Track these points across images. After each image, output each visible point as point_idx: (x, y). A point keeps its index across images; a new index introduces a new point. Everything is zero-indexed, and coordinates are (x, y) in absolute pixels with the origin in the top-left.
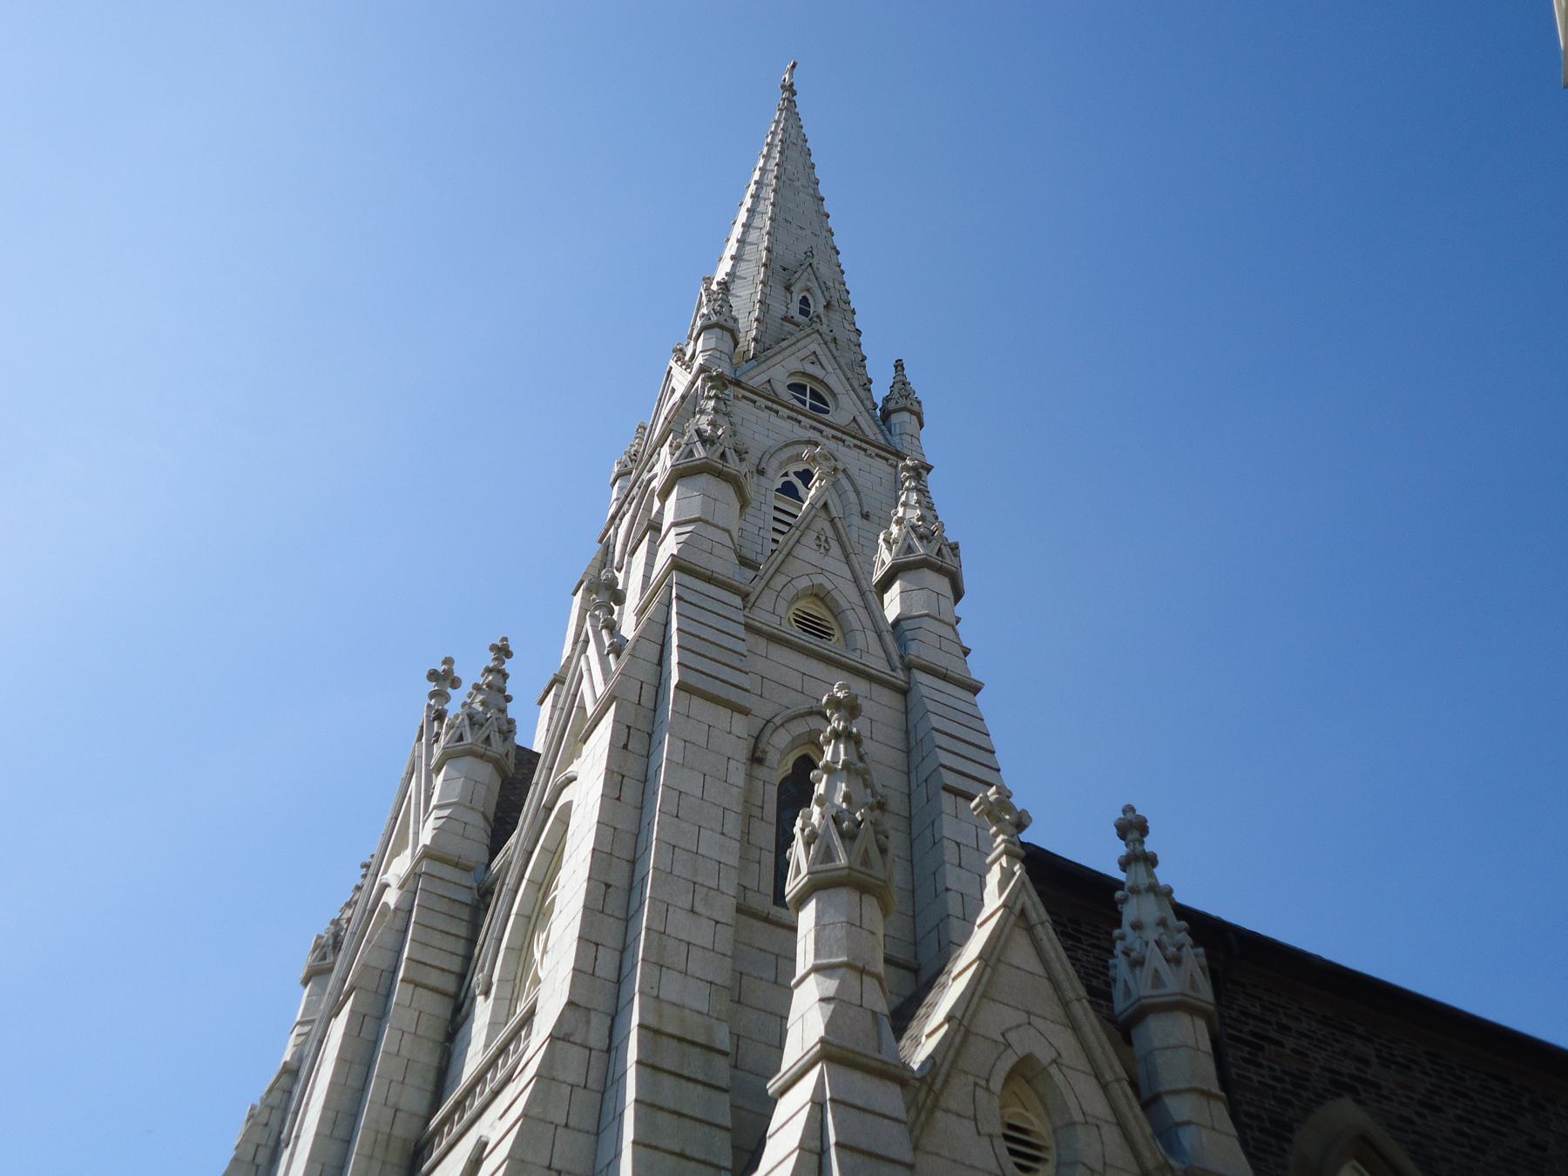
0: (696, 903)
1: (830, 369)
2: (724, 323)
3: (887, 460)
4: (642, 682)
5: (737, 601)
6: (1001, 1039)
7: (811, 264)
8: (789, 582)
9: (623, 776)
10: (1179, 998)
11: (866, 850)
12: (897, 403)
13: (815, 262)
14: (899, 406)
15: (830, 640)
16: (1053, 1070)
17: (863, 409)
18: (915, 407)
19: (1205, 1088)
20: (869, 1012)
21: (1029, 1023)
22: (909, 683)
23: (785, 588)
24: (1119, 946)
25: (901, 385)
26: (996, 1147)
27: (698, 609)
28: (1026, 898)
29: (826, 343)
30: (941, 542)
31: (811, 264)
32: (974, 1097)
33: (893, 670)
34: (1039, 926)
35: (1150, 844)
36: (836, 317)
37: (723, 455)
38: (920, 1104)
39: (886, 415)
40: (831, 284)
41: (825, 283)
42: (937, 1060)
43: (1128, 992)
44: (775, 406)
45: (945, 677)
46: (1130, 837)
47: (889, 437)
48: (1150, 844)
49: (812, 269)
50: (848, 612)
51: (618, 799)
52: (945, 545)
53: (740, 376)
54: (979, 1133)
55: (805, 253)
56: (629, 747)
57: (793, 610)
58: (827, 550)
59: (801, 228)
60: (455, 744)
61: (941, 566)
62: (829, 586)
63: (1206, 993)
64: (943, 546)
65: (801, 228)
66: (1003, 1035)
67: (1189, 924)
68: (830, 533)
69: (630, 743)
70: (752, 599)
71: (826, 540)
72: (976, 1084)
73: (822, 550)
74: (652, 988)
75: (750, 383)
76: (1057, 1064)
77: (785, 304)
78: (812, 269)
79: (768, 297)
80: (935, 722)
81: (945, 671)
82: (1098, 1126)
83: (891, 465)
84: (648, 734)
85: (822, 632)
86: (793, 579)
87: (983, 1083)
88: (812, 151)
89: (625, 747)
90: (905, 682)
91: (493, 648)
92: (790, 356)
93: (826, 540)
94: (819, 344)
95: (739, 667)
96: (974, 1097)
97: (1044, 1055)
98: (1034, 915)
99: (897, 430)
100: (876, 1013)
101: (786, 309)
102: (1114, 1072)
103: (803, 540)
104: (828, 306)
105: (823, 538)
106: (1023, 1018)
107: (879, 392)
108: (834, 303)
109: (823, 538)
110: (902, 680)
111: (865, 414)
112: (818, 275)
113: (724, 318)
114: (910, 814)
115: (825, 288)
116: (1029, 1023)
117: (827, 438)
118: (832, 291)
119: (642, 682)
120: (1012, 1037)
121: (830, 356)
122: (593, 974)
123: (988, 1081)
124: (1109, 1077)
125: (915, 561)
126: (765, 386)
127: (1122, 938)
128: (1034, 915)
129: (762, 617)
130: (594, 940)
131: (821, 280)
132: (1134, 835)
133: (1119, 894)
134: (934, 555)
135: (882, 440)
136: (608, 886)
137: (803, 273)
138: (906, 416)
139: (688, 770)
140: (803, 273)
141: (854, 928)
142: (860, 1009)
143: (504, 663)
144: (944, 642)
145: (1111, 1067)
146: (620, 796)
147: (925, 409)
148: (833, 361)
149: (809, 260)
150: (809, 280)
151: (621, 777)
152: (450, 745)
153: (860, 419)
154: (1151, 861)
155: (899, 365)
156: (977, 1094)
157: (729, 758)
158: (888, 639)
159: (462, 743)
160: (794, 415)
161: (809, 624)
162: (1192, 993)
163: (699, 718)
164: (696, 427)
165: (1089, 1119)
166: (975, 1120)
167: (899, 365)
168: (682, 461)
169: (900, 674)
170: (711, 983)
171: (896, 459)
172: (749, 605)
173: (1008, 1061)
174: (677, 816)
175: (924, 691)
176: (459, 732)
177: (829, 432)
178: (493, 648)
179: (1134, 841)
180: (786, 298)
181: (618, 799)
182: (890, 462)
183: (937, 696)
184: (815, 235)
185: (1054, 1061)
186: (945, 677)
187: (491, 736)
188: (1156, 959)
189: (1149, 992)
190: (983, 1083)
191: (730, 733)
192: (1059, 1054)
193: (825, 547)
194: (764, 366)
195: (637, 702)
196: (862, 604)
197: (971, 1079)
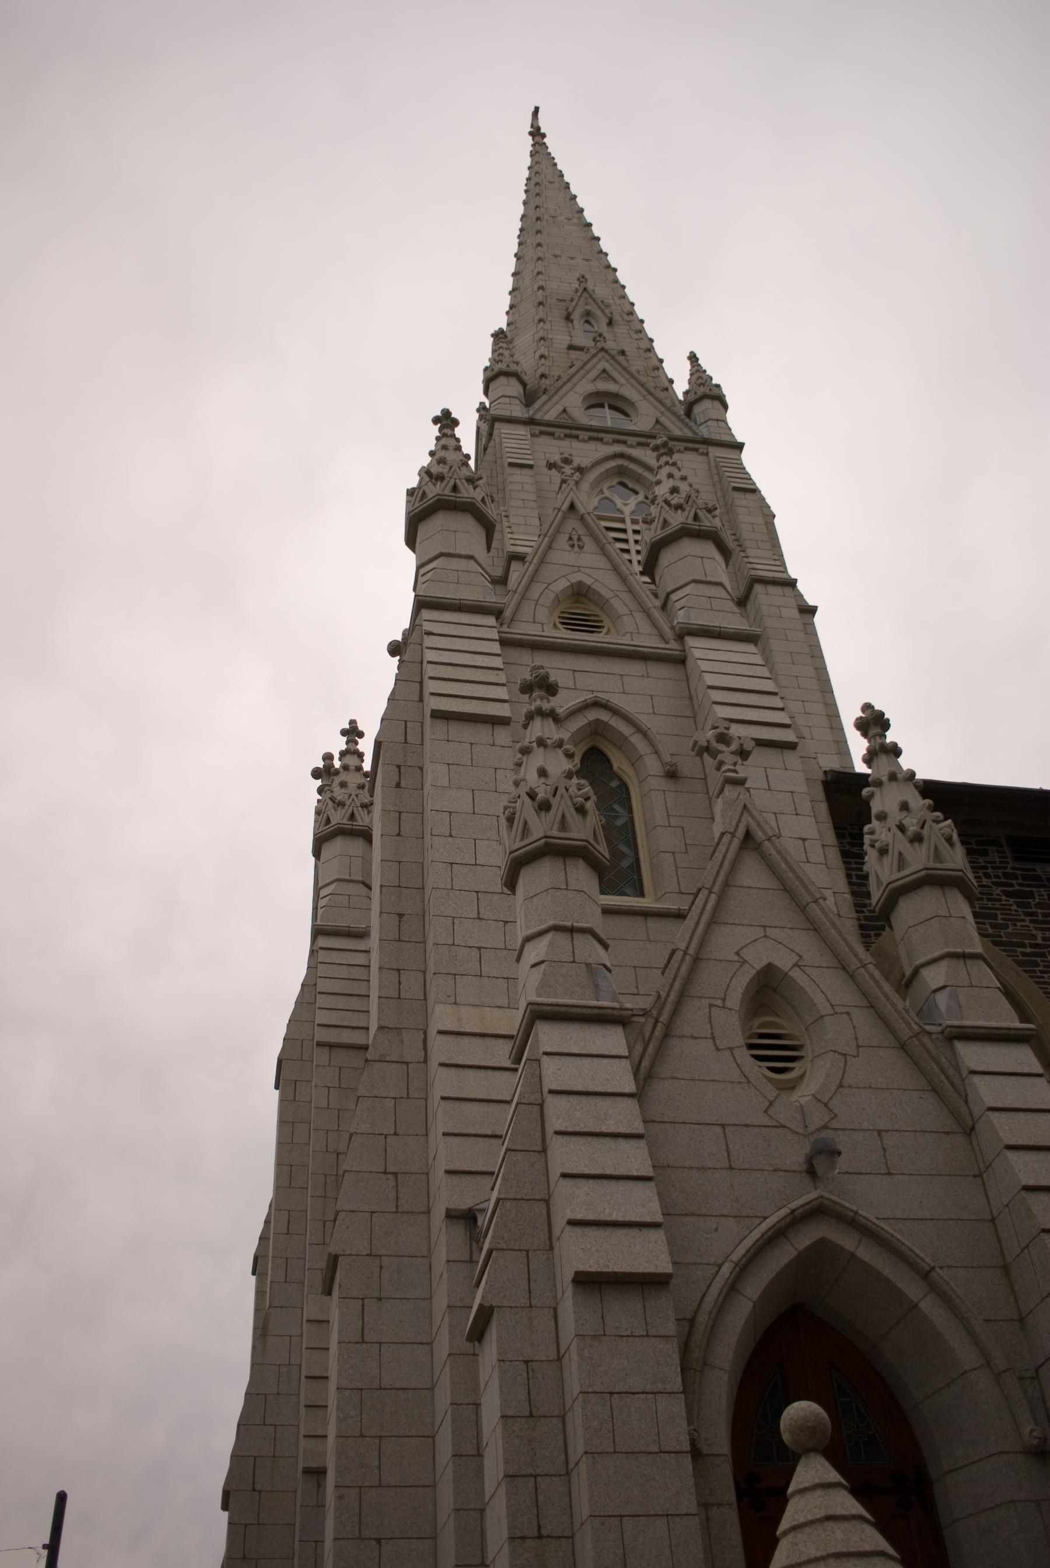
0: (482, 910)
1: (622, 381)
2: (507, 370)
3: (696, 450)
4: (406, 721)
5: (491, 621)
6: (736, 958)
7: (585, 289)
8: (546, 588)
9: (400, 813)
10: (924, 873)
11: (563, 817)
12: (696, 393)
13: (590, 286)
14: (697, 396)
15: (601, 632)
16: (795, 974)
17: (663, 409)
18: (715, 391)
19: (960, 950)
20: (583, 966)
21: (766, 936)
22: (684, 651)
23: (543, 596)
24: (867, 839)
25: (698, 374)
26: (737, 1057)
27: (449, 638)
28: (750, 819)
29: (613, 358)
30: (696, 507)
31: (585, 289)
32: (710, 1017)
33: (667, 643)
34: (766, 842)
35: (891, 737)
36: (621, 330)
37: (696, 517)
38: (647, 1035)
39: (689, 413)
40: (612, 301)
41: (603, 302)
42: (662, 993)
43: (879, 881)
44: (574, 432)
45: (459, 608)
46: (871, 733)
47: (695, 428)
48: (891, 737)
49: (588, 293)
50: (612, 601)
51: (399, 835)
52: (701, 509)
53: (534, 414)
54: (718, 1049)
55: (578, 279)
56: (403, 785)
57: (557, 613)
58: (581, 547)
59: (572, 258)
60: (325, 828)
61: (700, 530)
62: (588, 581)
63: (957, 859)
64: (698, 511)
65: (572, 258)
66: (737, 953)
67: (933, 801)
68: (581, 531)
69: (402, 781)
70: (508, 613)
71: (579, 539)
72: (711, 1006)
73: (576, 548)
74: (448, 996)
75: (547, 418)
76: (799, 966)
77: (568, 334)
78: (588, 293)
79: (549, 332)
80: (710, 680)
81: (719, 629)
82: (848, 1013)
83: (702, 454)
84: (419, 767)
85: (592, 625)
86: (549, 584)
87: (719, 1003)
88: (563, 172)
89: (398, 785)
90: (680, 651)
91: (344, 733)
92: (581, 380)
93: (579, 539)
94: (607, 361)
95: (495, 681)
96: (710, 1017)
97: (784, 961)
98: (760, 833)
99: (700, 419)
100: (590, 964)
101: (570, 338)
102: (860, 960)
103: (555, 545)
104: (610, 323)
105: (575, 538)
106: (760, 932)
107: (681, 386)
108: (617, 317)
109: (575, 538)
110: (676, 650)
111: (667, 413)
112: (594, 296)
113: (506, 365)
114: (705, 774)
115: (603, 306)
116: (766, 936)
117: (632, 446)
118: (613, 307)
119: (406, 721)
120: (745, 954)
121: (620, 369)
122: (399, 998)
123: (724, 1000)
124: (854, 964)
125: (672, 534)
126: (562, 416)
127: (872, 833)
128: (760, 833)
129: (525, 629)
130: (395, 968)
131: (599, 301)
132: (874, 730)
133: (865, 792)
134: (690, 521)
135: (690, 434)
136: (401, 916)
137: (579, 299)
138: (707, 404)
139: (455, 790)
140: (579, 299)
141: (559, 893)
142: (573, 964)
143: (357, 743)
144: (715, 602)
145: (856, 955)
146: (400, 831)
147: (725, 391)
148: (624, 373)
149: (583, 285)
150: (586, 304)
151: (398, 814)
152: (321, 830)
153: (663, 419)
154: (895, 751)
155: (693, 358)
156: (713, 1014)
157: (496, 769)
158: (656, 614)
159: (330, 825)
160: (595, 434)
161: (572, 622)
162: (938, 865)
163: (459, 740)
164: (664, 499)
165: (838, 1009)
166: (713, 1038)
167: (693, 358)
168: (418, 505)
169: (674, 645)
170: (507, 978)
171: (705, 446)
172: (507, 621)
173: (747, 976)
174: (451, 836)
175: (697, 653)
176: (325, 816)
177: (632, 440)
178: (344, 733)
179: (874, 736)
180: (568, 327)
181: (399, 835)
182: (701, 451)
183: (712, 655)
184: (587, 260)
185: (796, 965)
186: (459, 608)
187: (356, 812)
188: (901, 843)
189: (896, 875)
190: (719, 1003)
191: (494, 745)
192: (801, 957)
193: (578, 546)
194: (556, 398)
195: (403, 741)
196: (625, 588)
197: (705, 1002)
